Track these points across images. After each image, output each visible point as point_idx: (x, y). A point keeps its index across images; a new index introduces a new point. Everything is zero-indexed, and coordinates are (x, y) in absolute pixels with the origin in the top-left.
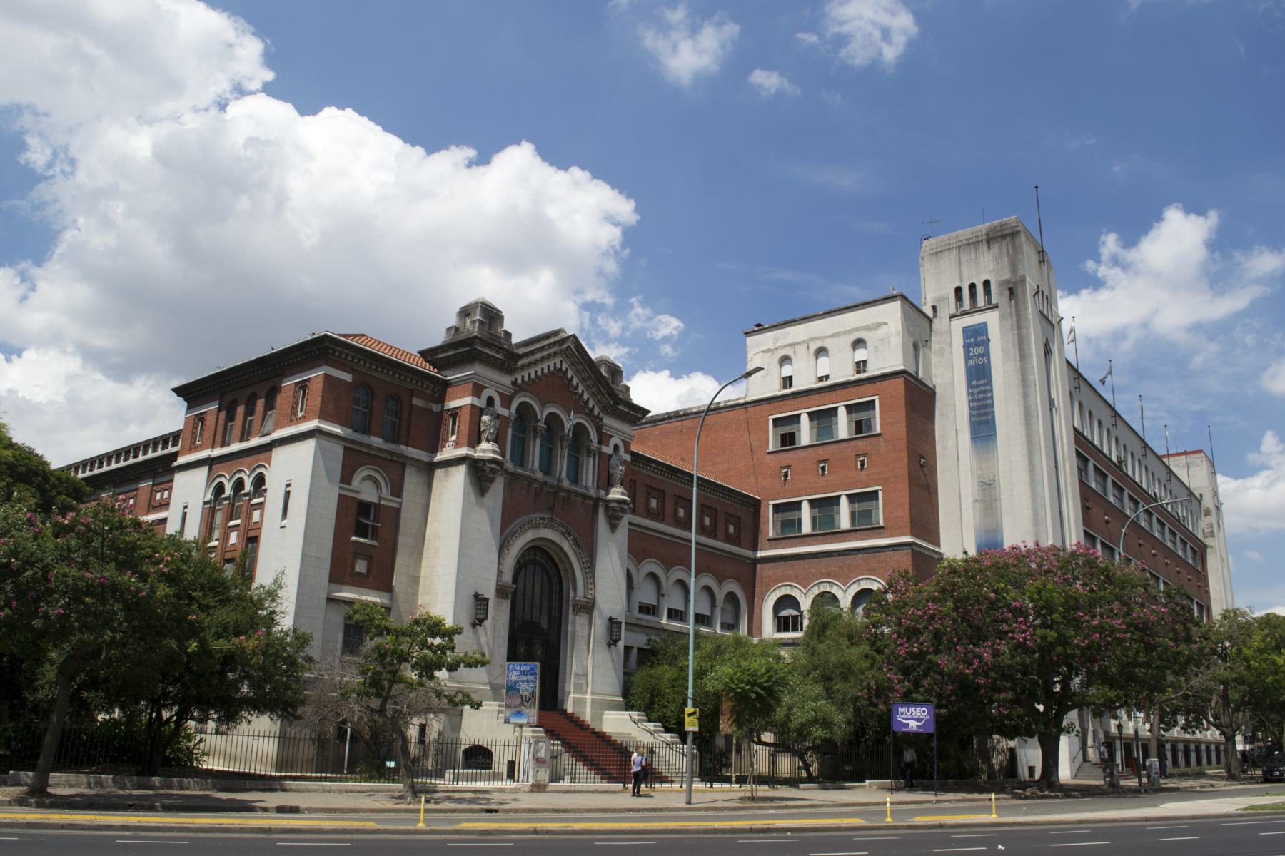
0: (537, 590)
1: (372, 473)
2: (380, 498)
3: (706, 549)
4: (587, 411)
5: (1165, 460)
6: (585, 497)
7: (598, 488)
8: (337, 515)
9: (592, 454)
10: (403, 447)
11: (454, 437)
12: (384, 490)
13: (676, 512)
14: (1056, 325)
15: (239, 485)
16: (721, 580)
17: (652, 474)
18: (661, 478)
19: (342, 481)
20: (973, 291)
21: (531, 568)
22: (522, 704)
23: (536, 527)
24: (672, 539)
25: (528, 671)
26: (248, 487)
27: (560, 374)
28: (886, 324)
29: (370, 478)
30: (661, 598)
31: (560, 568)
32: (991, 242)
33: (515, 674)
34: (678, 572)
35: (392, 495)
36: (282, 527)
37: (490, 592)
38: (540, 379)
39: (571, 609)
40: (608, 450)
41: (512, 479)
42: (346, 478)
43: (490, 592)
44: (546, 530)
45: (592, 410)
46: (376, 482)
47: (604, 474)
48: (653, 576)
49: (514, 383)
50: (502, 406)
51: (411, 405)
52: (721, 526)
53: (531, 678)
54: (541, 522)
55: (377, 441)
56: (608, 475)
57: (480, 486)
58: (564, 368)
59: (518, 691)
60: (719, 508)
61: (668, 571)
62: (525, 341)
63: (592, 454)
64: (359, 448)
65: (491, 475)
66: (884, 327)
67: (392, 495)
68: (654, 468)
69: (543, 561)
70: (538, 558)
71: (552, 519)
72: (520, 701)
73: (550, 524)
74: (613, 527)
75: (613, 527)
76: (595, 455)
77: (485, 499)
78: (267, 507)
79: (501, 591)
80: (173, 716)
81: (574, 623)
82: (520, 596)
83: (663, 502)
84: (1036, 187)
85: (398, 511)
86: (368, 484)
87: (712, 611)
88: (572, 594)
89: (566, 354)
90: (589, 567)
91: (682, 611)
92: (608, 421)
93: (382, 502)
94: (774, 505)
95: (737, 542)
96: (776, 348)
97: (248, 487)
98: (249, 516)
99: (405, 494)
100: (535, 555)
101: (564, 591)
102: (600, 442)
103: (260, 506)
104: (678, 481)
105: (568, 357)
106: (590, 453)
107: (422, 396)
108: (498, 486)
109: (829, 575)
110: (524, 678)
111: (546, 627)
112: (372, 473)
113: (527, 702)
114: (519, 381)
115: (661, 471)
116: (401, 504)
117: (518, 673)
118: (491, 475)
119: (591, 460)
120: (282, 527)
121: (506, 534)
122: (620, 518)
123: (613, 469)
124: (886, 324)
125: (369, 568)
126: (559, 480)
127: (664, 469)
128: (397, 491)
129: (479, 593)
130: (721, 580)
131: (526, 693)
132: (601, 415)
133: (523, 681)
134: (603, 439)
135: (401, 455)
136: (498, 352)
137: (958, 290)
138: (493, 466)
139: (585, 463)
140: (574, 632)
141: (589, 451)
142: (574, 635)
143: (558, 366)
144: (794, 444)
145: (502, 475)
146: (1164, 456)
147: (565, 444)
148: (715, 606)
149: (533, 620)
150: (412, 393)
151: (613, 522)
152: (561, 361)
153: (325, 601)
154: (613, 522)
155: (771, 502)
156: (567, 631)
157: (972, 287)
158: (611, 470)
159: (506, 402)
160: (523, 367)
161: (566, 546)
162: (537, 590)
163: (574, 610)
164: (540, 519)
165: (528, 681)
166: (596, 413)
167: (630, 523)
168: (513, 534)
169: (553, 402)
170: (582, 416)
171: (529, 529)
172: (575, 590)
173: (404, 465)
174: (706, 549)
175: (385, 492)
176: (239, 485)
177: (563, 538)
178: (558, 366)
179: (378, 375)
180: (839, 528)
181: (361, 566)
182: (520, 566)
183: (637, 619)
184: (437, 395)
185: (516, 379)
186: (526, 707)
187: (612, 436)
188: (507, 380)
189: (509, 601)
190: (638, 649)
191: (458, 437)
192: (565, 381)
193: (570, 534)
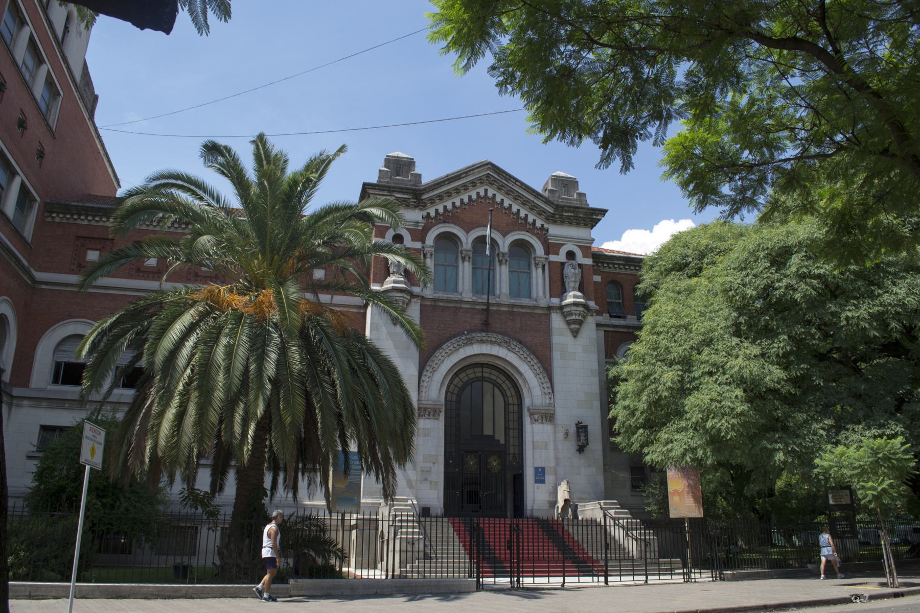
63: (540, 265)
70: (485, 375)
92: (556, 231)
102: (547, 252)
114: (433, 214)
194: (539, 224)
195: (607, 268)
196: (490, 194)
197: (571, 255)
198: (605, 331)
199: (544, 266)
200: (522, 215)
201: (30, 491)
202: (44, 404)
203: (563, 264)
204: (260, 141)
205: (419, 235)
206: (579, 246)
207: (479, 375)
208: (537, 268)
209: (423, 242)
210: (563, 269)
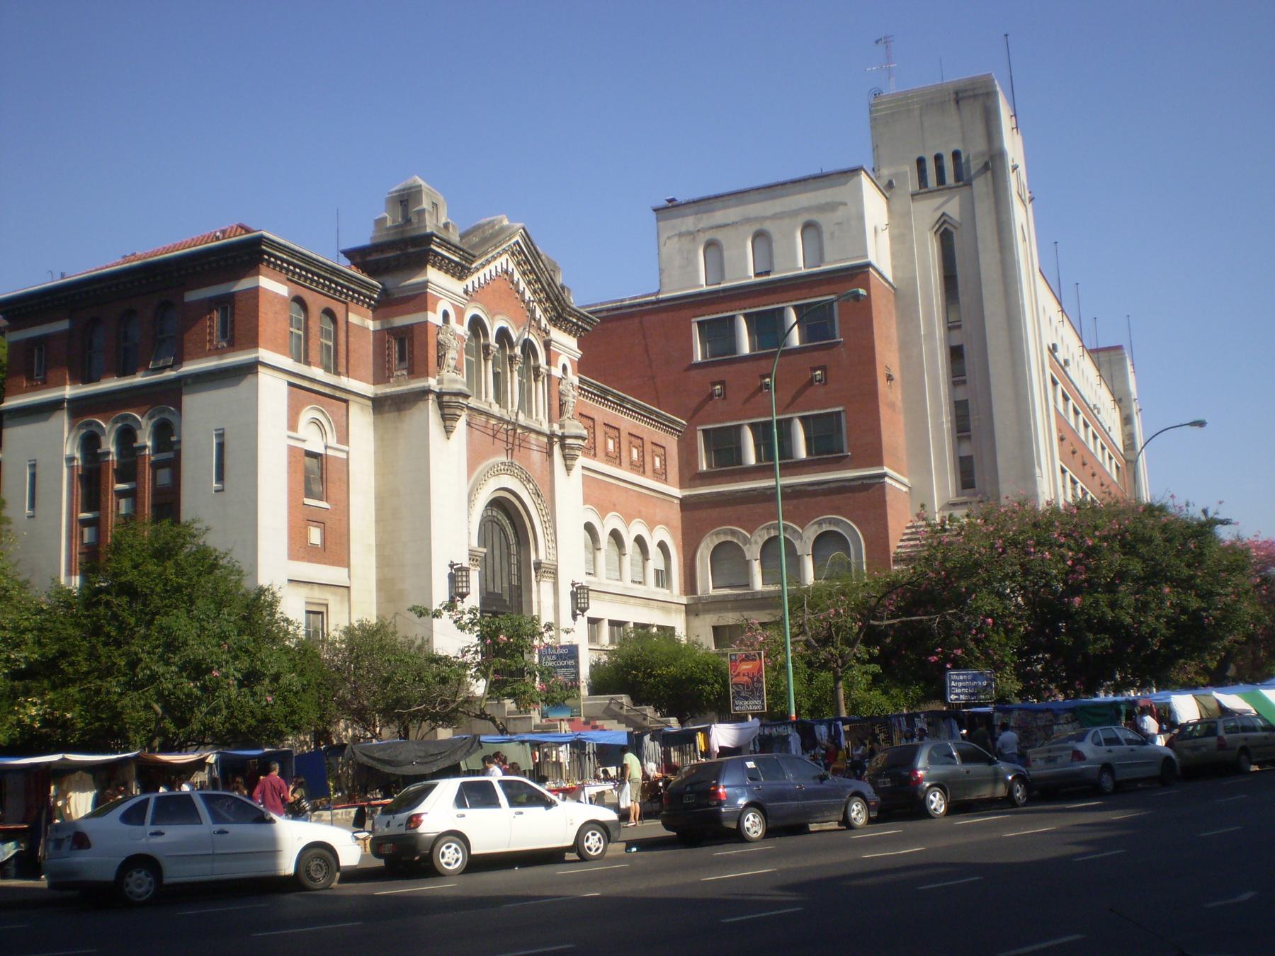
2: (326, 447)
7: (550, 421)
9: (541, 378)
12: (329, 434)
28: (845, 204)
32: (960, 102)
55: (318, 373)
57: (445, 427)
58: (510, 270)
61: (603, 519)
66: (841, 207)
80: (666, 755)
82: (489, 560)
84: (1006, 35)
86: (314, 428)
88: (533, 558)
90: (549, 521)
93: (330, 452)
96: (699, 231)
102: (549, 363)
114: (470, 289)
116: (348, 453)
124: (845, 204)
132: (548, 327)
133: (561, 667)
137: (921, 162)
143: (505, 267)
144: (735, 354)
147: (516, 367)
148: (647, 560)
154: (569, 462)
160: (477, 269)
165: (567, 666)
175: (332, 441)
178: (505, 267)
190: (635, 624)
198: (290, 384)
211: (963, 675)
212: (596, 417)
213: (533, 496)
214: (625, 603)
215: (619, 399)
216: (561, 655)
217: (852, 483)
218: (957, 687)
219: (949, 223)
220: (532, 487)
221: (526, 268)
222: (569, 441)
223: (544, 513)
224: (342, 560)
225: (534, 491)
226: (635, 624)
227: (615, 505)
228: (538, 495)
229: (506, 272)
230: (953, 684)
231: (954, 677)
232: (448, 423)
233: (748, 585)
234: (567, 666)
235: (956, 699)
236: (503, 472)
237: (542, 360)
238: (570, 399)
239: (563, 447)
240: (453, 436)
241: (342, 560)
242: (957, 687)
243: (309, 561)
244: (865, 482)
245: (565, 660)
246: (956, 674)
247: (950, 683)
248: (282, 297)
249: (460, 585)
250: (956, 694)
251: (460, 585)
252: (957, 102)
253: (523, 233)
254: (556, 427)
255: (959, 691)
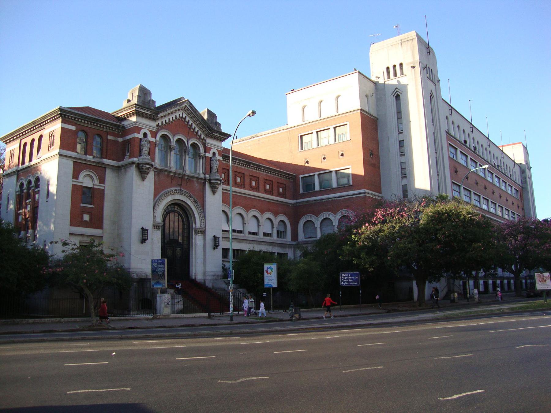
0: (176, 224)
1: (89, 173)
2: (94, 185)
3: (267, 200)
4: (198, 137)
5: (501, 148)
6: (199, 179)
8: (72, 194)
9: (202, 157)
10: (104, 160)
11: (129, 154)
13: (251, 183)
14: (436, 83)
15: (30, 182)
16: (276, 214)
17: (237, 166)
18: (242, 167)
19: (74, 178)
20: (395, 68)
21: (172, 215)
22: (159, 278)
23: (174, 194)
24: (249, 196)
25: (161, 263)
26: (33, 184)
27: (183, 119)
29: (88, 175)
30: (245, 225)
31: (188, 213)
33: (155, 264)
34: (253, 212)
35: (99, 183)
36: (47, 201)
37: (149, 226)
38: (172, 122)
39: (194, 232)
40: (209, 155)
41: (159, 172)
42: (76, 176)
43: (149, 226)
44: (178, 195)
45: (200, 136)
46: (91, 177)
47: (208, 167)
48: (269, 219)
49: (158, 125)
50: (152, 137)
51: (107, 139)
52: (275, 189)
53: (162, 266)
54: (175, 191)
56: (210, 167)
58: (184, 116)
59: (157, 272)
60: (274, 181)
61: (262, 214)
62: (195, 109)
63: (202, 157)
64: (81, 162)
65: (146, 171)
67: (99, 183)
68: (238, 163)
69: (181, 212)
70: (175, 209)
71: (181, 190)
72: (158, 277)
73: (180, 192)
74: (214, 193)
75: (214, 193)
76: (203, 158)
77: (145, 182)
78: (41, 192)
79: (156, 226)
81: (195, 239)
83: (244, 179)
85: (103, 191)
87: (272, 231)
88: (194, 226)
89: (185, 109)
91: (270, 234)
92: (209, 141)
93: (95, 187)
94: (302, 177)
95: (284, 196)
97: (33, 184)
98: (34, 197)
99: (106, 182)
100: (174, 208)
101: (190, 224)
102: (205, 152)
103: (38, 192)
104: (260, 171)
105: (186, 111)
106: (200, 157)
107: (113, 135)
108: (151, 176)
109: (328, 210)
110: (159, 266)
111: (181, 241)
112: (89, 173)
113: (161, 277)
114: (160, 124)
115: (242, 164)
116: (104, 187)
117: (157, 264)
118: (146, 171)
119: (201, 160)
120: (47, 201)
121: (157, 198)
122: (217, 188)
123: (212, 164)
125: (91, 218)
126: (199, 174)
127: (243, 163)
128: (102, 181)
129: (144, 227)
130: (276, 214)
131: (160, 273)
132: (205, 138)
134: (206, 150)
135: (103, 163)
136: (148, 111)
137: (388, 68)
138: (147, 166)
139: (198, 162)
140: (196, 243)
141: (200, 156)
142: (196, 245)
143: (181, 115)
145: (153, 170)
146: (500, 147)
148: (274, 227)
149: (175, 239)
150: (108, 133)
151: (213, 190)
152: (183, 113)
153: (69, 234)
154: (213, 190)
155: (301, 176)
156: (192, 243)
157: (394, 66)
158: (211, 165)
159: (154, 134)
160: (162, 117)
161: (189, 202)
162: (176, 224)
163: (195, 233)
164: (175, 190)
166: (202, 137)
167: (223, 189)
168: (160, 199)
169: (179, 133)
170: (195, 139)
171: (169, 195)
172: (195, 223)
173: (105, 168)
174: (267, 200)
175: (96, 182)
176: (30, 182)
177: (187, 199)
178: (181, 115)
179: (89, 126)
180: (332, 187)
181: (86, 217)
182: (167, 213)
183: (248, 237)
184: (120, 133)
185: (159, 123)
186: (161, 280)
187: (211, 148)
188: (153, 124)
189: (161, 230)
190: (277, 253)
191: (130, 153)
192: (185, 123)
193: (191, 197)
194: (202, 136)
195: (105, 129)
196: (184, 116)
197: (145, 135)
198: (74, 161)
199: (203, 158)
200: (196, 130)
201: (193, 277)
202: (248, 242)
203: (141, 139)
204: (209, 112)
205: (154, 134)
206: (150, 131)
207: (173, 209)
208: (200, 158)
209: (156, 138)
210: (141, 142)
211: (347, 274)
212: (245, 173)
213: (194, 202)
214: (259, 244)
215: (257, 166)
216: (159, 263)
217: (353, 196)
218: (344, 279)
219: (399, 92)
220: (192, 199)
221: (192, 116)
222: (212, 181)
223: (199, 209)
224: (100, 226)
225: (194, 200)
226: (277, 253)
227: (255, 206)
228: (196, 202)
229: (182, 117)
230: (343, 277)
231: (343, 275)
232: (143, 175)
233: (316, 237)
234: (161, 267)
235: (344, 284)
236: (176, 193)
237: (202, 151)
238: (215, 165)
239: (210, 183)
240: (147, 180)
241: (100, 226)
242: (344, 279)
243: (82, 227)
244: (358, 195)
245: (160, 265)
246: (344, 274)
247: (342, 277)
248: (73, 131)
249: (145, 236)
250: (344, 282)
251: (145, 236)
252: (401, 44)
253: (188, 102)
254: (207, 176)
255: (345, 281)
